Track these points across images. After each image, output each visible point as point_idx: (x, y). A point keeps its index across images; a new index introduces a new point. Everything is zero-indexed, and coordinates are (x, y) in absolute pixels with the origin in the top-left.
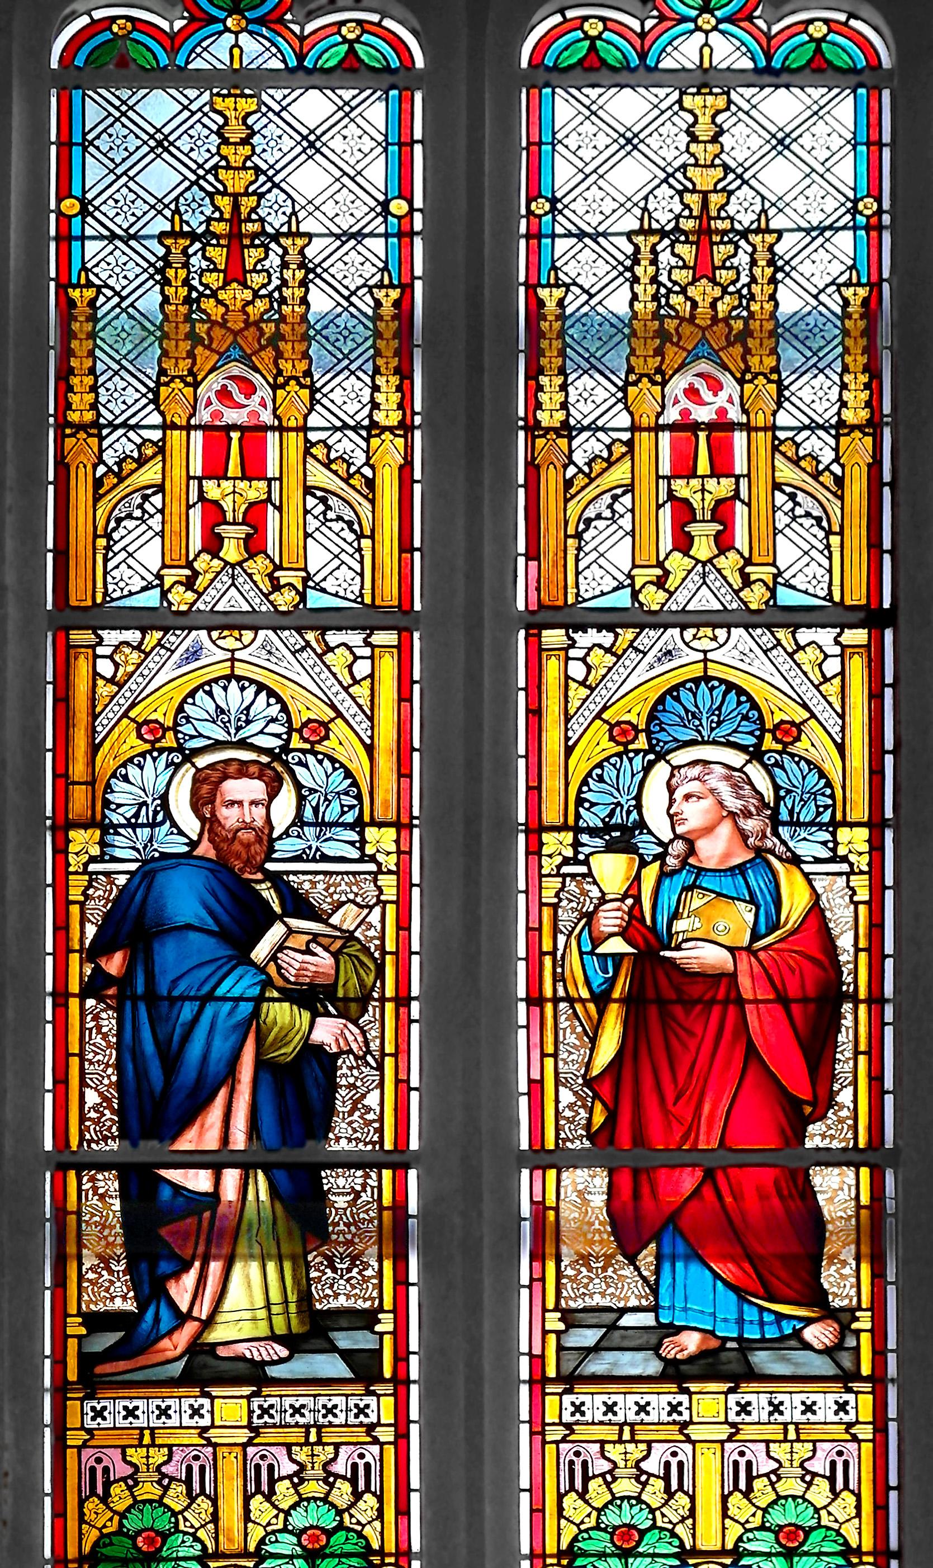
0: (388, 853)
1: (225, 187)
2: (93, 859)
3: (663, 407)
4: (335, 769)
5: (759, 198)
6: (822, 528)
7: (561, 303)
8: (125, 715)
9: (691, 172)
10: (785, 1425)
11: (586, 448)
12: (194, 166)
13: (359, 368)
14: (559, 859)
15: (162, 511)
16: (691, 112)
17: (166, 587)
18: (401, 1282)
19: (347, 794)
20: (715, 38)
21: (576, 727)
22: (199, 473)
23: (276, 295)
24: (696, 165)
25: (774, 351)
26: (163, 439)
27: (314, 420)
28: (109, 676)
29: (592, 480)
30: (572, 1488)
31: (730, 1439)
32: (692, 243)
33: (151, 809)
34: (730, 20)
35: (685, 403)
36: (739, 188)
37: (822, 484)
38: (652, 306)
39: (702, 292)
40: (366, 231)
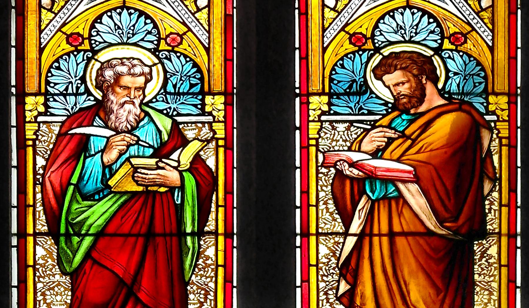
0: (503, 110)
2: (40, 114)
4: (187, 62)
8: (59, 30)
14: (35, 113)
19: (478, 75)
21: (329, 35)
28: (332, 7)
33: (74, 86)
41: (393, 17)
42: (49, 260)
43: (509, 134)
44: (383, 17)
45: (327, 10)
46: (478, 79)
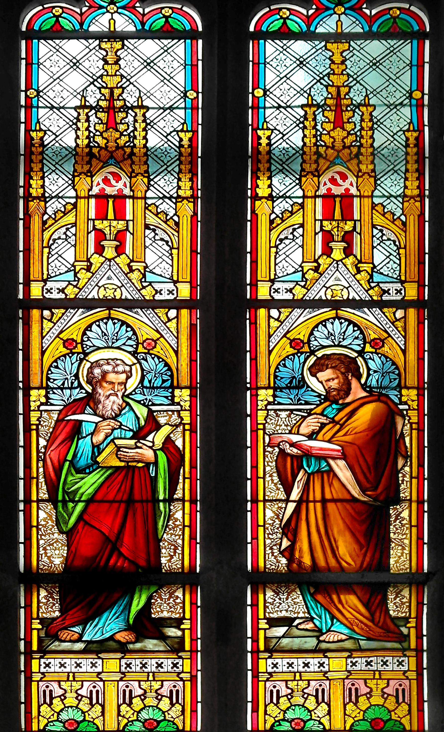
1: (333, 83)
3: (318, 187)
4: (160, 362)
5: (364, 90)
6: (169, 246)
7: (269, 138)
8: (58, 336)
9: (105, 78)
10: (148, 673)
11: (53, 206)
12: (91, 75)
13: (173, 169)
14: (266, 402)
15: (75, 235)
16: (104, 49)
17: (305, 271)
18: (420, 604)
20: (116, 16)
22: (94, 217)
23: (132, 134)
24: (107, 75)
25: (372, 162)
26: (303, 203)
27: (376, 193)
28: (276, 317)
29: (56, 221)
30: (45, 702)
31: (121, 680)
32: (105, 112)
33: (70, 382)
34: (123, 8)
35: (329, 185)
36: (355, 85)
37: (169, 225)
38: (86, 142)
39: (338, 134)
40: (175, 106)
41: (325, 326)
42: (49, 521)
43: (191, 420)
44: (317, 326)
45: (272, 320)
46: (393, 376)
